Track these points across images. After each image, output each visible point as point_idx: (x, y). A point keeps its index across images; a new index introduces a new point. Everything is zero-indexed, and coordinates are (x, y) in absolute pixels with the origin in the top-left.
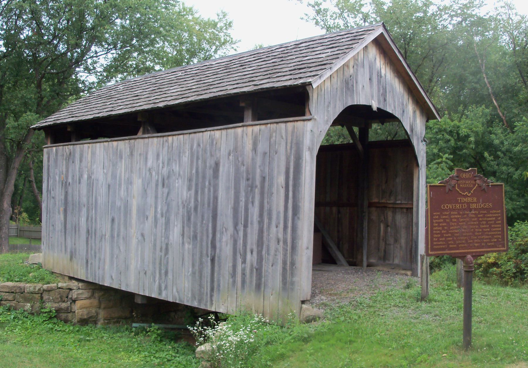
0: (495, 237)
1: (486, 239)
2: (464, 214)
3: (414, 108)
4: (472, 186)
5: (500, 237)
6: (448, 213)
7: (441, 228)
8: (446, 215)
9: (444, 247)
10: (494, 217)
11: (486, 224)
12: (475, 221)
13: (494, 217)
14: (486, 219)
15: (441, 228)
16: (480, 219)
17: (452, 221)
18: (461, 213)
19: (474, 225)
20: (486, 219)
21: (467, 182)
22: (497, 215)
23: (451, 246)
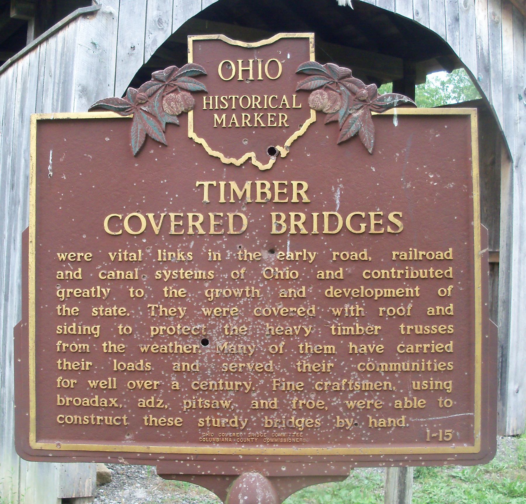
0: (416, 385)
1: (361, 395)
2: (237, 263)
3: (494, 14)
4: (283, 120)
5: (449, 386)
6: (138, 256)
7: (96, 330)
8: (128, 265)
9: (110, 420)
10: (412, 282)
11: (363, 321)
12: (299, 301)
13: (412, 282)
14: (363, 291)
15: (96, 330)
16: (332, 292)
17: (158, 296)
18: (215, 256)
19: (294, 320)
20: (363, 291)
21: (253, 102)
22: (434, 272)
23: (150, 419)
